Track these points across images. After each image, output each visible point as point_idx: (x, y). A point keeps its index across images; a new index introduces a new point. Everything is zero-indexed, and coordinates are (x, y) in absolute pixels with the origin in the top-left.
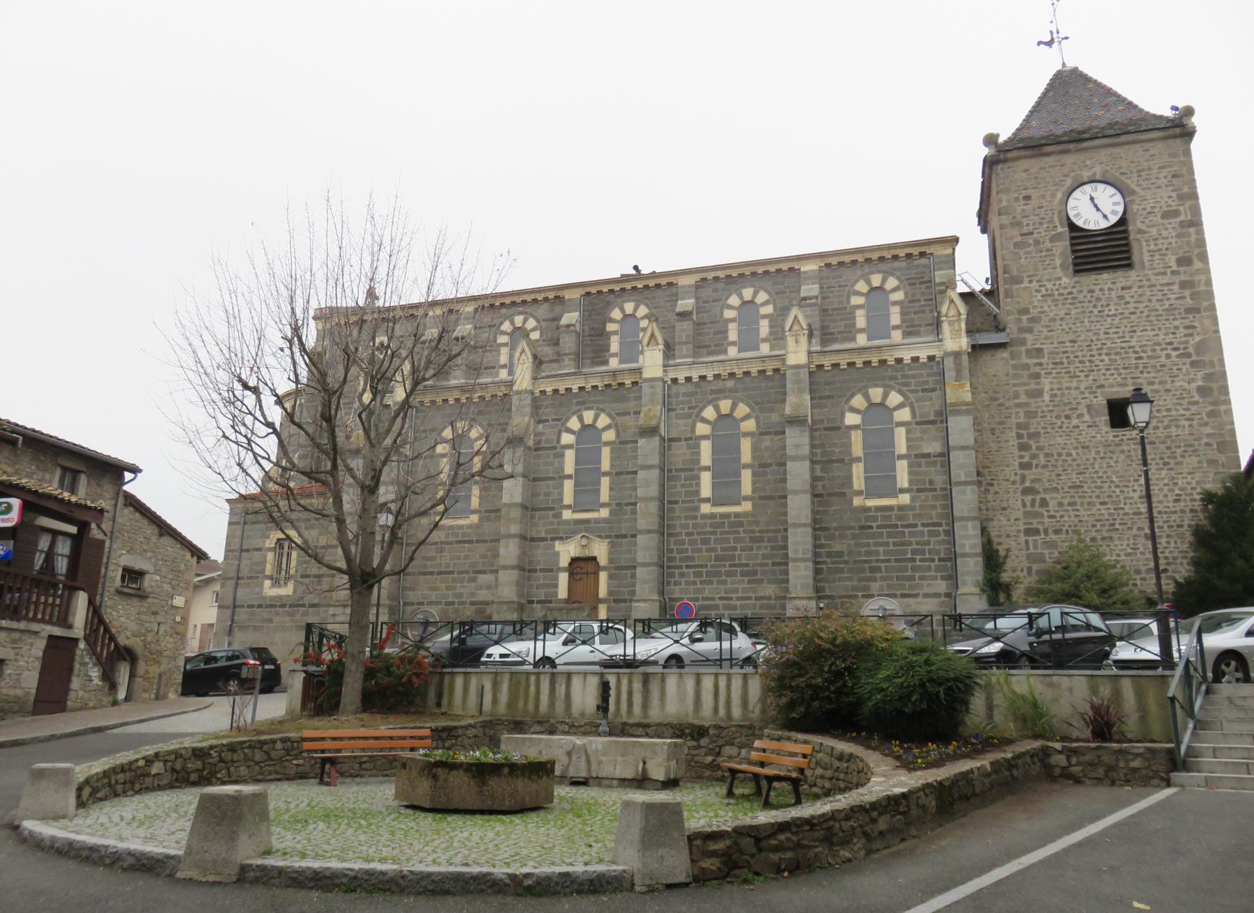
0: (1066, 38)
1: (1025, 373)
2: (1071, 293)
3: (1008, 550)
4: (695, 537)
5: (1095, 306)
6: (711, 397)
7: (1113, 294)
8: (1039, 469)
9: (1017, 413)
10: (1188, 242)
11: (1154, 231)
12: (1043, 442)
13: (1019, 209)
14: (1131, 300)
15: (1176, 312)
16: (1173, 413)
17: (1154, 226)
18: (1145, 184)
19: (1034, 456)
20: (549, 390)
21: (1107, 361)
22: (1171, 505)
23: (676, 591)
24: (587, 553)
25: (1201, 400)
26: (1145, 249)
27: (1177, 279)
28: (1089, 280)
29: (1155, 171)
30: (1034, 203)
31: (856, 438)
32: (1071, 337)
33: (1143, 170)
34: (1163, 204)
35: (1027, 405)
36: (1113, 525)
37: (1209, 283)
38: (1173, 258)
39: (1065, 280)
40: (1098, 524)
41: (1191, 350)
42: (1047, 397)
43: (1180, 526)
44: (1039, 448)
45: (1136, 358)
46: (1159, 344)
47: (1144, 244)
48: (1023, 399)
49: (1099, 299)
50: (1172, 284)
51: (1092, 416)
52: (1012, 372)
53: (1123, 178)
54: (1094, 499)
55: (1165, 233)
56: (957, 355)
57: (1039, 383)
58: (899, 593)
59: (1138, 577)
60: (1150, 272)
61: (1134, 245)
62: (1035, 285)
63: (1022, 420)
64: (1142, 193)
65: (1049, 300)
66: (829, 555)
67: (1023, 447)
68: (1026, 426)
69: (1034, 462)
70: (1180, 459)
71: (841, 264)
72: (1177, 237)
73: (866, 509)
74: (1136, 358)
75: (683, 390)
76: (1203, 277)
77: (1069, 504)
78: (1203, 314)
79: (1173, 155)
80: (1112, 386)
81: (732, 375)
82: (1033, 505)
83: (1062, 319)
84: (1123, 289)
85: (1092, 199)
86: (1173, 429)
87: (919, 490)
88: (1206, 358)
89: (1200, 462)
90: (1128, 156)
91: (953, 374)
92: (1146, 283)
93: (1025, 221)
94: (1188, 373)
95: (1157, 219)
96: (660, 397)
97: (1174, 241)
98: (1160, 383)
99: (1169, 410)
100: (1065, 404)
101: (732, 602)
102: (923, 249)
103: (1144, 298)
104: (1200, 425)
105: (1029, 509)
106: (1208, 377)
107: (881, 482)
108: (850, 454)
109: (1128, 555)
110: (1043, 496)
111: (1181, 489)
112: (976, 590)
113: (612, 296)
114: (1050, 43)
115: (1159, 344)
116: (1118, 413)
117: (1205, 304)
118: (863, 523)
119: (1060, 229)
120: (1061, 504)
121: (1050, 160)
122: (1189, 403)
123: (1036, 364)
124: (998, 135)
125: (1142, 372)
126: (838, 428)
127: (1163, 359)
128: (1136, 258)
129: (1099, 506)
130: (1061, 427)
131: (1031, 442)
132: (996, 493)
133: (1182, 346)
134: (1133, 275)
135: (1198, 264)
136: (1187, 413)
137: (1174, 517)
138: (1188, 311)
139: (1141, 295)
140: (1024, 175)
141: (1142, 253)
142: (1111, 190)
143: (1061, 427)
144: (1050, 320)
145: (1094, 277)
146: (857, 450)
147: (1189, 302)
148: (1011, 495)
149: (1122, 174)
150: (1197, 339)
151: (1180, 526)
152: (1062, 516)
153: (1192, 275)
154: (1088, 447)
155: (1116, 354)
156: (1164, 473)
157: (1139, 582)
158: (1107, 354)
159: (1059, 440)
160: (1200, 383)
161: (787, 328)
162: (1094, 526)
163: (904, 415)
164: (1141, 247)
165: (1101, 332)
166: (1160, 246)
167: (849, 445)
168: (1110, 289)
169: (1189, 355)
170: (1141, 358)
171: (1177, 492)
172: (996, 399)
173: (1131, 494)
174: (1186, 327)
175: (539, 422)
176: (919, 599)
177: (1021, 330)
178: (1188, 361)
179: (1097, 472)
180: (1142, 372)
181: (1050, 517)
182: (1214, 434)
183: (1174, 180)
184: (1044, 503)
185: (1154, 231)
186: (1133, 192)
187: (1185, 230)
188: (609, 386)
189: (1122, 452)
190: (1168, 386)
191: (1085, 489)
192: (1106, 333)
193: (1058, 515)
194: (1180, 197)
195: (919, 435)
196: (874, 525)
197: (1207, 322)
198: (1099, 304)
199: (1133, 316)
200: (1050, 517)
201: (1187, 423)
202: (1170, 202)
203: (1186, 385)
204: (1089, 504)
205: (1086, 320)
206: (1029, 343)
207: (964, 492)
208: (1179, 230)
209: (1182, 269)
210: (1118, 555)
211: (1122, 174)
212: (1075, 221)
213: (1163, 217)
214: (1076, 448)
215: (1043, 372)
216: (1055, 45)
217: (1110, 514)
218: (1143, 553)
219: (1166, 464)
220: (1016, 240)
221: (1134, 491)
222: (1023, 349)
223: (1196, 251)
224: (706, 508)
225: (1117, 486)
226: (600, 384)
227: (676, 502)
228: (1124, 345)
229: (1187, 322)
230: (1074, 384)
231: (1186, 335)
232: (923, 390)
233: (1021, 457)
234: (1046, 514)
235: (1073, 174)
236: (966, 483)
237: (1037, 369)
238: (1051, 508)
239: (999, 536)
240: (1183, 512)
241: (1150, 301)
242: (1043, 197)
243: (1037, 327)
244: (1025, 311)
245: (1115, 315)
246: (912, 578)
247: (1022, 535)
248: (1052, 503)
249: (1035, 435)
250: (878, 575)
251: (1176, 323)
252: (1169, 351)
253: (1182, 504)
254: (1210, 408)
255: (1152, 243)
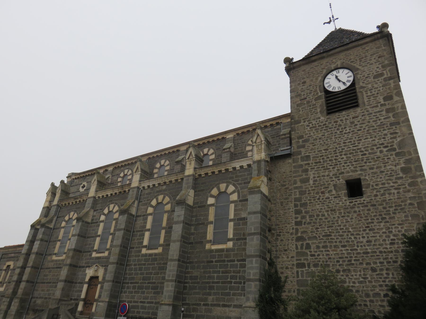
0: (337, 19)
1: (300, 170)
2: (325, 124)
3: (287, 277)
4: (236, 262)
5: (338, 129)
6: (156, 194)
7: (348, 122)
8: (306, 225)
9: (295, 192)
10: (389, 88)
11: (370, 86)
12: (309, 208)
13: (300, 89)
14: (358, 123)
15: (385, 126)
16: (386, 185)
17: (370, 83)
18: (363, 64)
19: (304, 217)
20: (101, 196)
21: (345, 159)
22: (388, 246)
23: (125, 297)
24: (96, 275)
25: (404, 176)
26: (365, 95)
27: (384, 108)
28: (334, 116)
29: (368, 58)
30: (308, 84)
31: (212, 211)
32: (326, 147)
33: (363, 58)
34: (374, 71)
35: (301, 187)
36: (350, 261)
37: (404, 107)
38: (381, 98)
39: (322, 118)
40: (341, 260)
41: (395, 146)
42: (311, 182)
43: (395, 262)
44: (306, 212)
45: (362, 155)
46: (376, 145)
47: (364, 93)
48: (299, 184)
49: (340, 125)
50: (382, 111)
51: (337, 191)
52: (293, 169)
53: (352, 64)
54: (338, 244)
55: (376, 86)
56: (259, 162)
57: (307, 175)
58: (221, 303)
59: (368, 299)
60: (368, 107)
61: (359, 95)
62: (307, 123)
63: (298, 196)
64: (362, 69)
65: (314, 129)
66: (191, 278)
67: (298, 212)
68: (299, 200)
69: (304, 221)
70: (392, 215)
71: (243, 133)
72: (382, 86)
73: (211, 251)
74: (362, 155)
75: (147, 192)
76: (400, 105)
77: (323, 247)
78: (402, 125)
79: (378, 48)
80: (348, 172)
81: (165, 183)
82: (302, 248)
83: (320, 139)
84: (353, 118)
85: (336, 77)
86: (387, 195)
87: (237, 240)
88: (405, 150)
89: (406, 216)
90: (353, 54)
91: (256, 172)
92: (366, 113)
93: (302, 93)
94: (395, 160)
95: (371, 79)
96: (135, 195)
97: (381, 88)
98: (377, 168)
99: (383, 184)
100: (321, 185)
101: (145, 305)
102: (277, 121)
103: (365, 121)
104: (405, 192)
105: (299, 250)
106: (408, 161)
107: (221, 237)
108: (208, 220)
109: (361, 282)
110: (307, 242)
111: (394, 235)
112: (253, 304)
113: (158, 158)
114: (329, 23)
115: (376, 145)
116: (355, 188)
117: (402, 119)
118: (209, 259)
119: (320, 94)
120: (318, 247)
121: (316, 63)
122: (396, 178)
123: (306, 164)
124: (292, 59)
125: (366, 163)
126: (204, 206)
127: (378, 154)
128: (360, 101)
129: (341, 248)
130: (319, 199)
131: (302, 209)
132: (282, 240)
133: (389, 145)
134: (359, 110)
135: (396, 98)
136: (396, 185)
137: (391, 255)
138: (391, 124)
139: (364, 120)
140: (303, 73)
141: (363, 98)
142: (346, 71)
143: (319, 199)
144: (314, 140)
145: (337, 114)
146: (211, 218)
147: (392, 119)
148: (290, 241)
149: (352, 62)
150: (399, 139)
151: (395, 262)
152: (319, 255)
153: (393, 104)
154: (335, 210)
155: (350, 154)
156: (382, 224)
157: (368, 303)
158: (345, 155)
159: (318, 207)
160: (403, 165)
161: (187, 158)
162: (338, 261)
163: (234, 197)
164: (363, 95)
165: (342, 143)
166: (373, 93)
167: (207, 215)
168: (346, 119)
169: (394, 150)
170: (365, 154)
171: (392, 237)
172: (285, 185)
173: (361, 239)
174: (391, 134)
175: (95, 211)
176: (231, 309)
177: (299, 147)
178: (394, 153)
179: (340, 226)
180: (366, 163)
181: (312, 255)
182: (415, 197)
183: (380, 59)
184: (308, 246)
185: (370, 86)
186: (358, 69)
187: (387, 82)
188: (120, 192)
189: (355, 212)
190: (382, 169)
191: (333, 237)
192: (344, 143)
193: (316, 254)
194: (383, 67)
195: (240, 207)
196: (214, 260)
197: (404, 129)
198: (340, 128)
199: (359, 132)
200: (312, 255)
201: (396, 191)
202: (378, 70)
203: (394, 168)
204: (335, 246)
205: (333, 137)
206: (303, 154)
207: (252, 239)
208: (384, 83)
209: (386, 103)
210: (354, 283)
211: (352, 62)
212: (328, 89)
213: (374, 78)
214: (328, 211)
215: (309, 168)
216: (332, 23)
217: (348, 254)
218: (370, 282)
219: (383, 219)
220: (298, 103)
221: (363, 237)
222: (299, 157)
223: (395, 92)
224: (144, 251)
225: (352, 235)
226: (117, 192)
227: (133, 248)
228: (354, 148)
229: (392, 131)
230: (327, 173)
231: (391, 138)
232: (244, 183)
233: (296, 218)
234: (309, 253)
235: (326, 67)
236: (254, 234)
237: (307, 167)
238: (312, 250)
239: (282, 268)
240: (397, 251)
241: (369, 122)
242: (312, 80)
243: (307, 144)
244: (302, 137)
245: (349, 132)
246: (228, 294)
247: (295, 267)
248: (313, 246)
249: (304, 205)
250: (213, 291)
251: (385, 132)
252: (382, 149)
253: (396, 246)
254: (410, 181)
255: (369, 92)
